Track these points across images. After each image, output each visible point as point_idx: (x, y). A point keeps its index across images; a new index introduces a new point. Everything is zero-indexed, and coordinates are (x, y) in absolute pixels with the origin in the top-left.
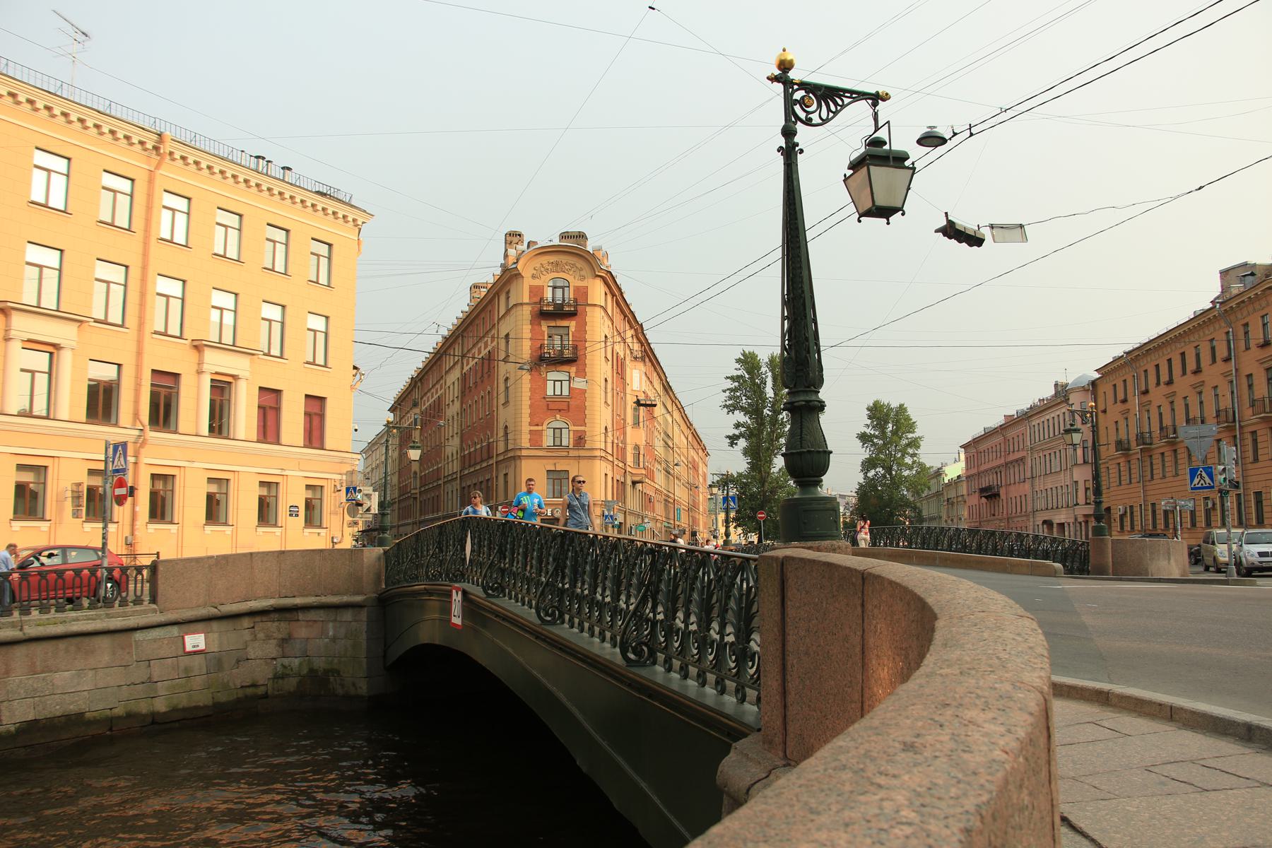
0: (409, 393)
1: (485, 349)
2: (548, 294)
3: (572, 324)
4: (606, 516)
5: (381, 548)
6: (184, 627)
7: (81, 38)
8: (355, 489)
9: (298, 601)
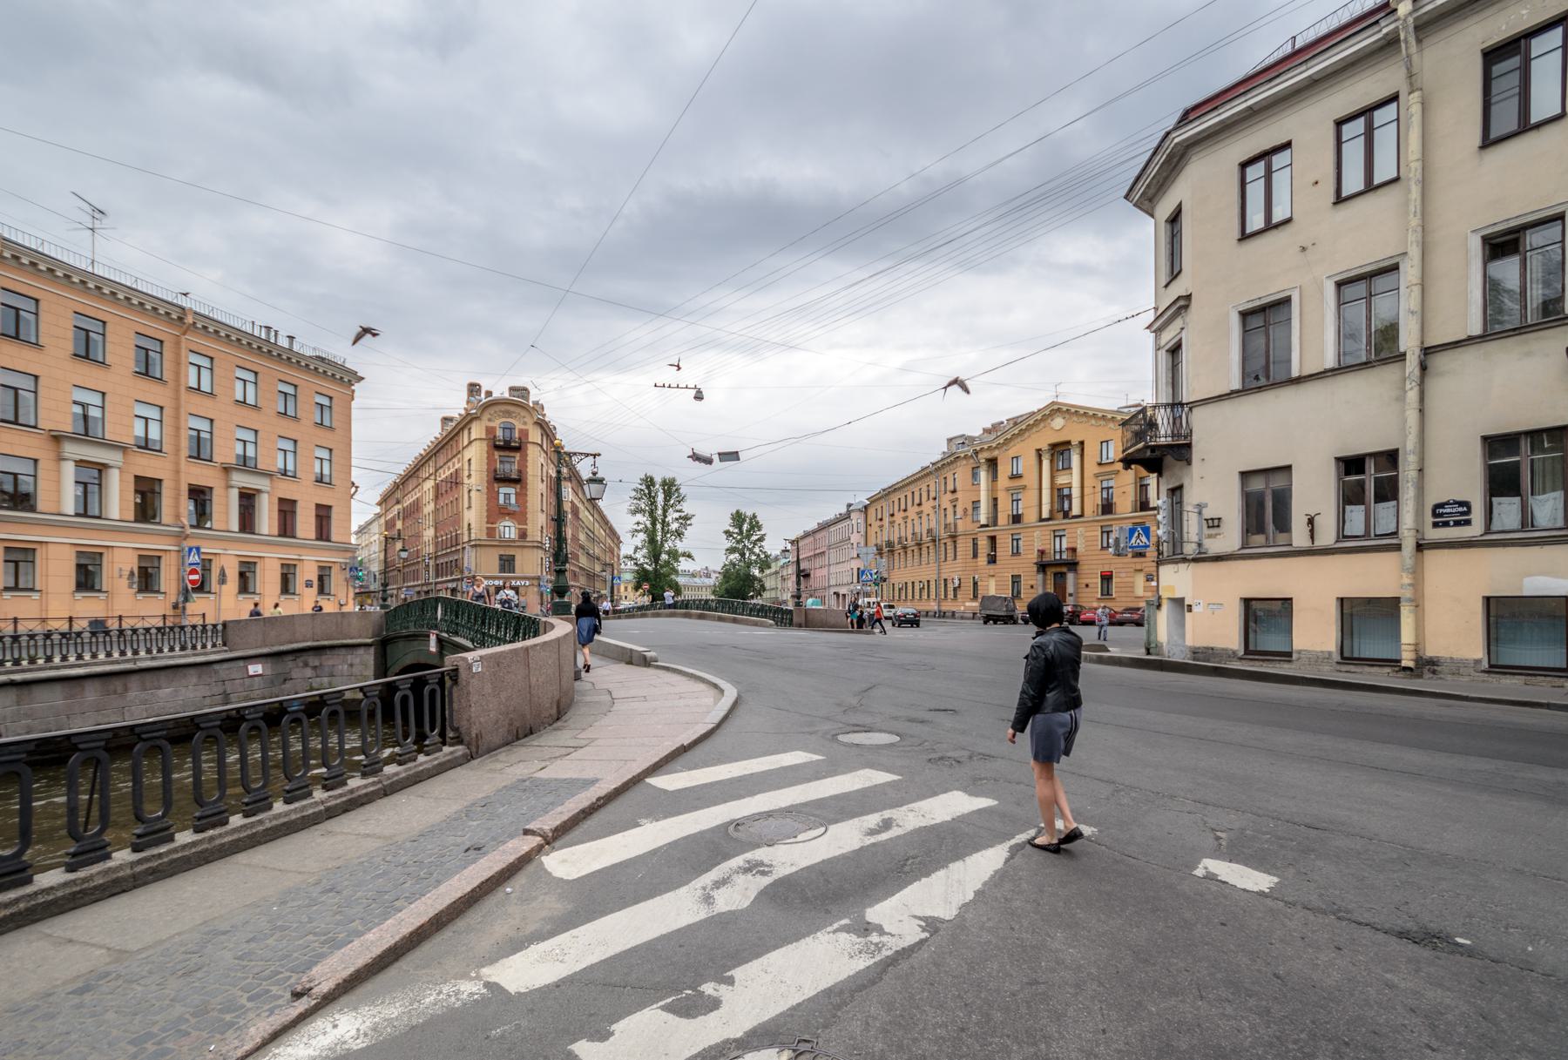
2: (499, 433)
3: (518, 455)
6: (249, 661)
7: (97, 215)
8: (356, 569)
9: (326, 643)
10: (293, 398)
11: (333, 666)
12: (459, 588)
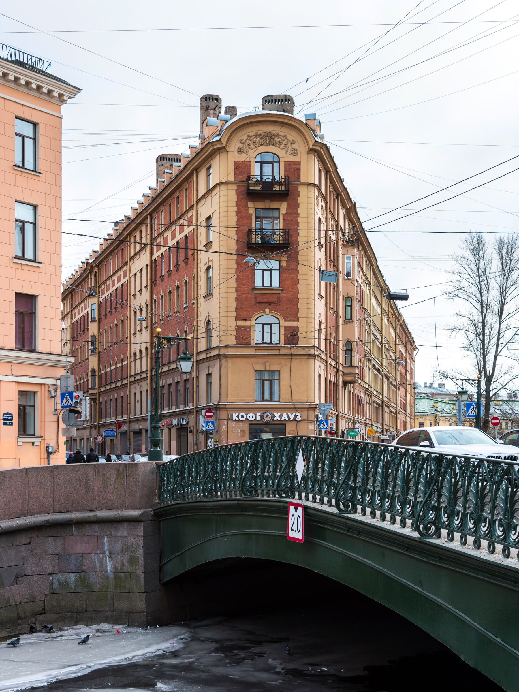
0: (84, 280)
1: (180, 233)
2: (256, 171)
3: (283, 206)
4: (321, 421)
5: (154, 462)
10: (31, 141)
11: (83, 555)
12: (192, 424)
